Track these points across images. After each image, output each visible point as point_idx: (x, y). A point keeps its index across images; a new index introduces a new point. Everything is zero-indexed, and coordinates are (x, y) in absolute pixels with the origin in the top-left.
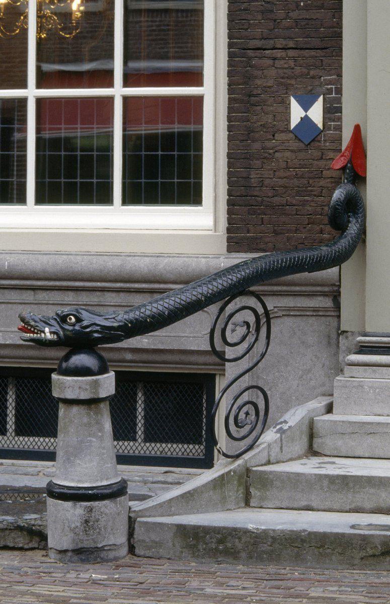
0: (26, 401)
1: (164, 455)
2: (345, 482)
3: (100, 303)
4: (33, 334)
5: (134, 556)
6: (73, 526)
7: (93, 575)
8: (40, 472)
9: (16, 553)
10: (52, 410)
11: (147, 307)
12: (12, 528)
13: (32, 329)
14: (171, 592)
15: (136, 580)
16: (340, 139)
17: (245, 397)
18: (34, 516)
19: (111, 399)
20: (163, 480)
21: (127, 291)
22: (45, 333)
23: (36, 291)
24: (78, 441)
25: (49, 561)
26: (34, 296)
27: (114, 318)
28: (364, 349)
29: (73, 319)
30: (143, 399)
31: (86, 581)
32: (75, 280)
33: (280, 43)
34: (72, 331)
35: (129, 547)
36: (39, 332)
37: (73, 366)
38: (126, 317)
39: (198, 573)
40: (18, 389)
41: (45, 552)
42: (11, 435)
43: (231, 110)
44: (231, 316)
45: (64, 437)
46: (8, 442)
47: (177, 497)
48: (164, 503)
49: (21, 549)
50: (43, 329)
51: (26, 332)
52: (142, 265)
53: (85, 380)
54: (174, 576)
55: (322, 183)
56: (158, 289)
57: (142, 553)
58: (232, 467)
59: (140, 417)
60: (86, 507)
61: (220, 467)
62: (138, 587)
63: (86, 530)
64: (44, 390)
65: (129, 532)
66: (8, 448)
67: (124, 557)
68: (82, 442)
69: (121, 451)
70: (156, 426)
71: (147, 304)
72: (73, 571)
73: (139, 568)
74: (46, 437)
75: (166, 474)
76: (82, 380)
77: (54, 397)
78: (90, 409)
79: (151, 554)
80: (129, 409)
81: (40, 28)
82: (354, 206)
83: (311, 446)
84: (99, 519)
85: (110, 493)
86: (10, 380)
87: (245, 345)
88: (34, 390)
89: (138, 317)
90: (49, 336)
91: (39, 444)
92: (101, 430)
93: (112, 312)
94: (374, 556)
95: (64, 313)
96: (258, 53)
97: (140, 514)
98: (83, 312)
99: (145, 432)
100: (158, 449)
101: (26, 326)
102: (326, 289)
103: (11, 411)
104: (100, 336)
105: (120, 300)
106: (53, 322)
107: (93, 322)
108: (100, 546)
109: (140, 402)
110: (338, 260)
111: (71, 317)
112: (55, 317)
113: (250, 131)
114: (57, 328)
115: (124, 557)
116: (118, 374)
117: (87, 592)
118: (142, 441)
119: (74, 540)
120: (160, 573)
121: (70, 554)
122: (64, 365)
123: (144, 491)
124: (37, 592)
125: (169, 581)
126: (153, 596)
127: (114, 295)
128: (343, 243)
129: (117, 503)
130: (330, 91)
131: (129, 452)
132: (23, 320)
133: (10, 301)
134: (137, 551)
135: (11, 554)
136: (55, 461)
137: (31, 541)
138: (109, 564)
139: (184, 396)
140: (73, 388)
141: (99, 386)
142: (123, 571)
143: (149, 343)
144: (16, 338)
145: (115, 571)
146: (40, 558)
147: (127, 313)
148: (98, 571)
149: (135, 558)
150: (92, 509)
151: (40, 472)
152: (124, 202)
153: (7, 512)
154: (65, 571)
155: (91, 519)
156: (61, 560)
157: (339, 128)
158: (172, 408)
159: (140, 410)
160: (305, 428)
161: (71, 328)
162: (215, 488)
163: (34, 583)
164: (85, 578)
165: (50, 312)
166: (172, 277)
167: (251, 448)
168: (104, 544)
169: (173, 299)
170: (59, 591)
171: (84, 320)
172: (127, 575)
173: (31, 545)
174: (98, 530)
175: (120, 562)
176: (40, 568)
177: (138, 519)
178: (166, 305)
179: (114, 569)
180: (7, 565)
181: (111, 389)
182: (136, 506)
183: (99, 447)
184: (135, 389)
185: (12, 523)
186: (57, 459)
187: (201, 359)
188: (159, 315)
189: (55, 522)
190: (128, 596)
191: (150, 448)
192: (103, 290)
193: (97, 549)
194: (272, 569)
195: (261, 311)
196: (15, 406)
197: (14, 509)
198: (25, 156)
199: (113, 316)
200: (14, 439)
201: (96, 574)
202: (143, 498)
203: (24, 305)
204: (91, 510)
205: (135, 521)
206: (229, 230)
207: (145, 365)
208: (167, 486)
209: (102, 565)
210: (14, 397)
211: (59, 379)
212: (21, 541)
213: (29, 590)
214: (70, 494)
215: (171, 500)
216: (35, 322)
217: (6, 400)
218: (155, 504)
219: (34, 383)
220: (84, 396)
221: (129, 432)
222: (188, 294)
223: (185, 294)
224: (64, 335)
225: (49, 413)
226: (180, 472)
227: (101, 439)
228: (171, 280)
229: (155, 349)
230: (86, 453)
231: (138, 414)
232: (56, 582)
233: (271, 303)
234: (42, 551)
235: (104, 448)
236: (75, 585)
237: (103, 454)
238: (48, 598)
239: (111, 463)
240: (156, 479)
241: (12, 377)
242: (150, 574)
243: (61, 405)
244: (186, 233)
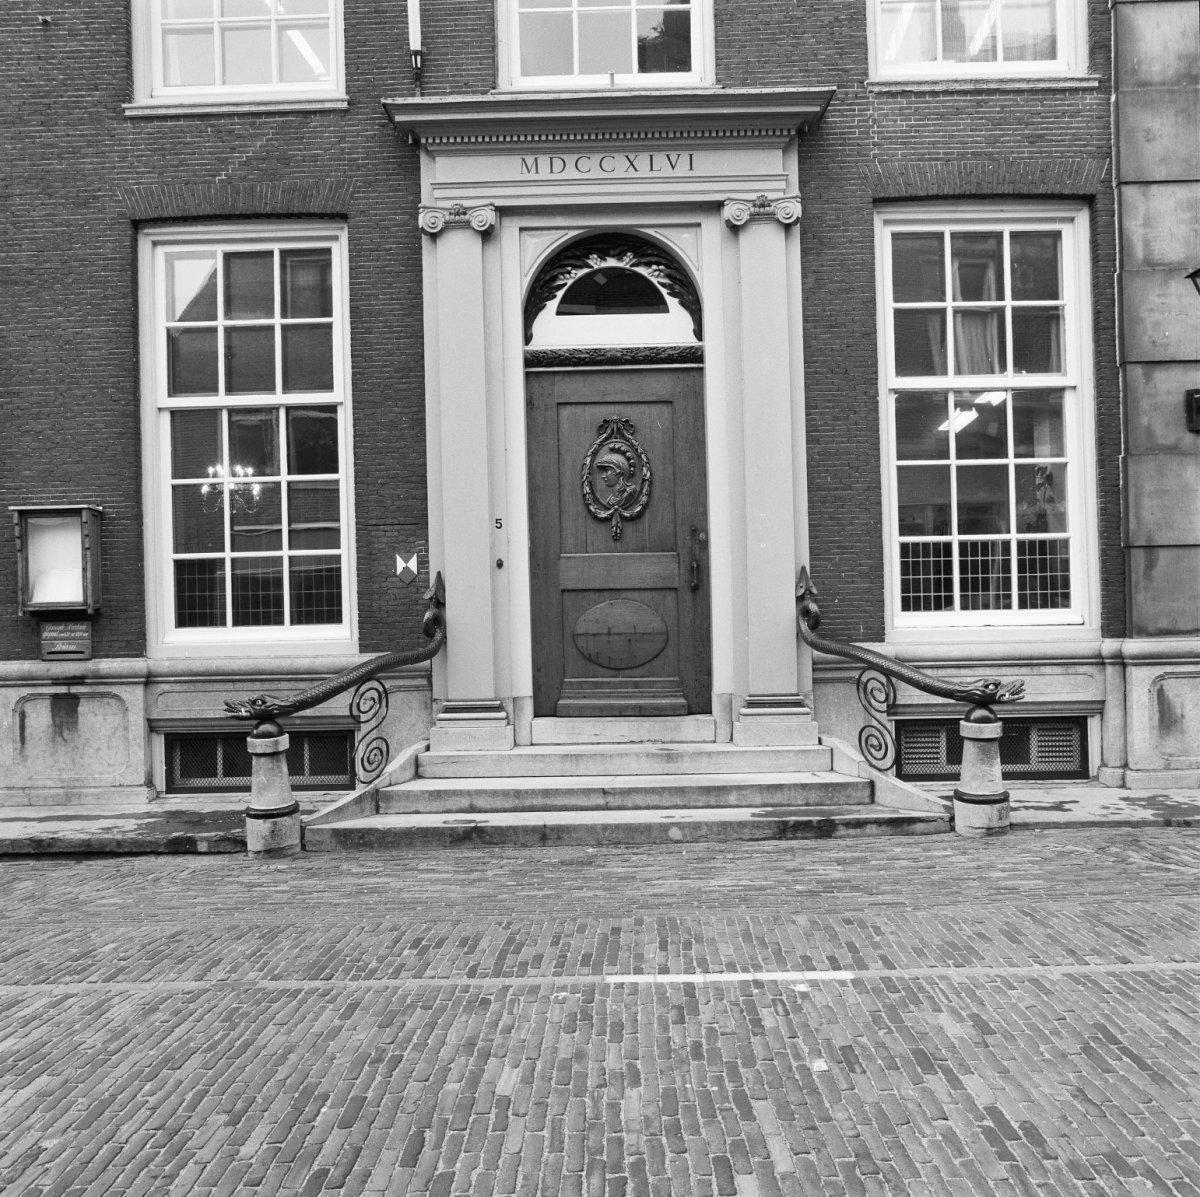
2: (438, 795)
16: (428, 580)
17: (374, 744)
19: (286, 752)
28: (448, 710)
33: (390, 521)
39: (347, 859)
43: (358, 563)
44: (363, 694)
49: (230, 853)
52: (304, 663)
61: (360, 789)
81: (232, 507)
82: (439, 621)
90: (244, 714)
92: (281, 772)
93: (286, 695)
110: (430, 655)
113: (371, 577)
114: (249, 708)
116: (167, 736)
123: (311, 807)
128: (432, 645)
130: (421, 551)
132: (227, 704)
152: (292, 623)
157: (428, 573)
158: (327, 752)
160: (413, 762)
165: (246, 697)
167: (378, 776)
182: (305, 818)
187: (345, 721)
194: (394, 853)
195: (381, 689)
198: (233, 591)
201: (281, 865)
202: (310, 812)
220: (269, 751)
230: (269, 787)
242: (317, 862)
244: (334, 643)
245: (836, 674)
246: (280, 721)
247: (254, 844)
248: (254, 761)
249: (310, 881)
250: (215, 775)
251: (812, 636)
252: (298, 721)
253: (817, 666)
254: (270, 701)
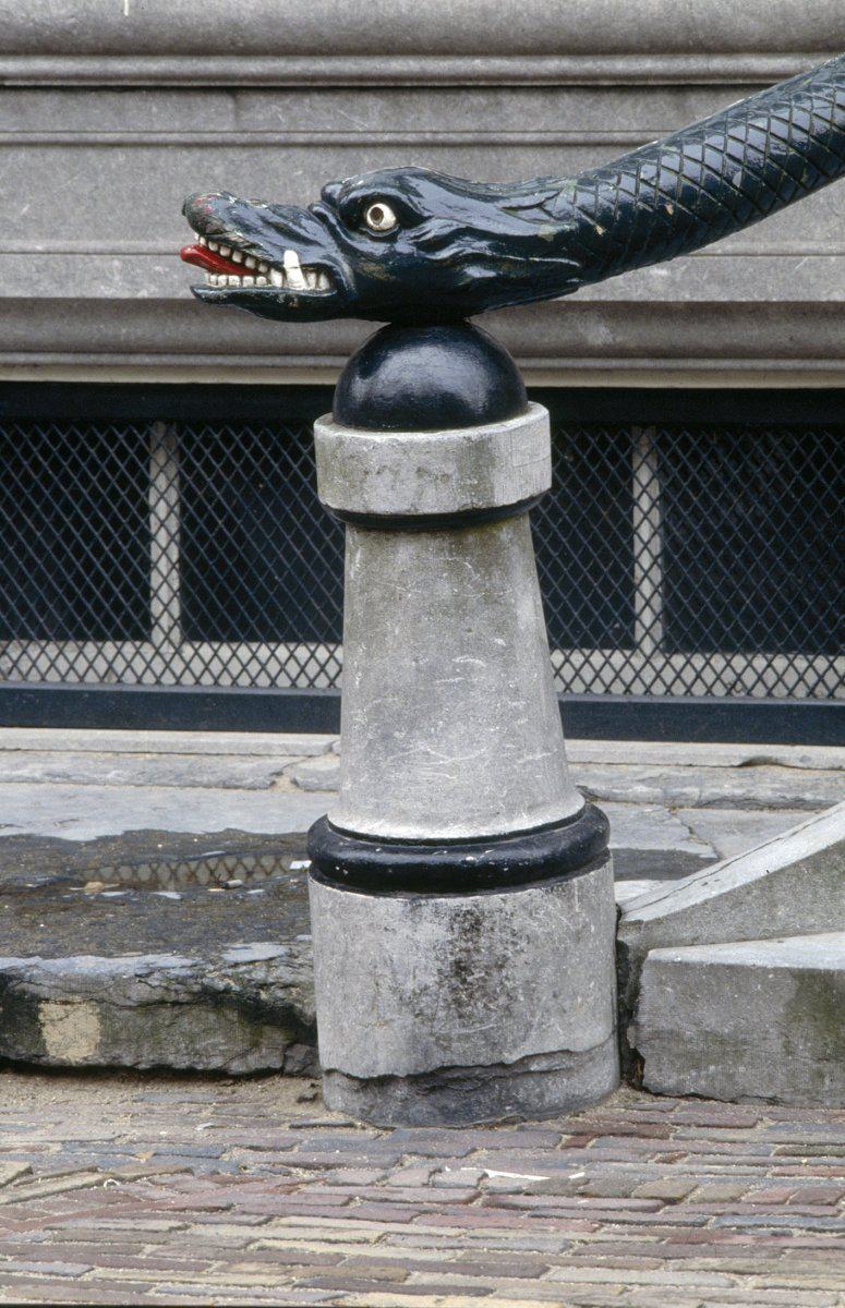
0: (220, 509)
1: (739, 697)
3: (484, 137)
4: (241, 276)
5: (639, 1094)
6: (410, 985)
7: (492, 1173)
8: (279, 774)
9: (201, 1091)
10: (318, 540)
11: (665, 160)
12: (183, 997)
13: (236, 258)
14: (784, 1235)
15: (651, 1188)
19: (537, 510)
20: (738, 792)
21: (586, 88)
22: (283, 272)
23: (246, 99)
24: (418, 670)
25: (325, 1119)
26: (237, 115)
27: (540, 206)
29: (389, 217)
30: (655, 491)
31: (463, 1195)
32: (390, 49)
34: (384, 259)
35: (622, 1058)
36: (262, 269)
37: (391, 392)
38: (586, 199)
40: (189, 467)
41: (308, 1083)
42: (167, 637)
45: (368, 655)
46: (158, 666)
47: (795, 865)
48: (747, 888)
49: (218, 1076)
50: (276, 257)
51: (212, 270)
53: (441, 443)
54: (793, 1169)
56: (704, 77)
57: (670, 1082)
59: (646, 560)
60: (456, 914)
62: (659, 1216)
63: (458, 1003)
64: (286, 467)
65: (620, 1002)
66: (157, 689)
67: (606, 1097)
68: (432, 672)
69: (578, 687)
70: (707, 588)
71: (663, 147)
72: (414, 1158)
73: (662, 1138)
74: (299, 642)
75: (750, 769)
76: (429, 443)
77: (319, 509)
78: (462, 549)
79: (702, 1085)
80: (605, 528)
84: (506, 959)
85: (544, 858)
86: (158, 432)
88: (247, 467)
89: (630, 199)
91: (273, 668)
93: (527, 177)
95: (353, 195)
97: (658, 932)
98: (424, 187)
99: (666, 616)
100: (718, 678)
101: (213, 247)
103: (164, 551)
104: (491, 274)
105: (561, 124)
106: (312, 229)
107: (464, 226)
108: (511, 1057)
109: (645, 503)
111: (380, 206)
112: (322, 210)
114: (327, 249)
115: (606, 1097)
117: (473, 1243)
118: (657, 647)
119: (414, 1039)
120: (739, 1159)
121: (401, 1091)
122: (360, 387)
123: (668, 839)
124: (283, 1245)
125: (777, 1192)
126: (716, 1255)
127: (535, 102)
129: (570, 897)
131: (607, 691)
132: (199, 223)
133: (146, 138)
134: (651, 1074)
135: (179, 1098)
136: (339, 733)
137: (255, 1045)
138: (549, 1124)
139: (808, 474)
140: (396, 473)
141: (494, 466)
142: (603, 1153)
143: (673, 283)
144: (182, 281)
145: (570, 1154)
146: (290, 1110)
147: (591, 184)
148: (510, 1154)
149: (647, 1101)
150: (478, 922)
151: (279, 774)
153: (160, 938)
154: (387, 1158)
155: (476, 957)
156: (368, 1118)
159: (645, 531)
161: (379, 249)
163: (270, 1209)
164: (459, 1187)
165: (303, 183)
166: (755, 29)
168: (526, 1049)
169: (762, 123)
170: (366, 1241)
171: (430, 217)
172: (616, 1170)
173: (254, 1062)
174: (502, 1000)
175: (585, 1119)
176: (290, 1148)
177: (652, 954)
178: (736, 149)
179: (566, 1147)
180: (170, 1141)
181: (536, 472)
182: (640, 897)
183: (499, 692)
184: (623, 456)
185: (181, 981)
186: (354, 609)
188: (712, 187)
189: (342, 973)
190: (623, 1253)
191: (689, 675)
192: (494, 86)
196: (181, 530)
197: (189, 925)
199: (538, 198)
200: (178, 651)
202: (673, 867)
203: (197, 153)
204: (476, 926)
205: (640, 960)
207: (662, 363)
208: (755, 815)
209: (522, 1129)
210: (173, 496)
211: (341, 442)
212: (218, 1044)
213: (252, 1241)
214: (397, 867)
215: (772, 878)
216: (247, 229)
217: (146, 510)
218: (715, 893)
219: (247, 440)
220: (436, 501)
221: (607, 616)
222: (817, 103)
223: (807, 104)
224: (357, 276)
225: (309, 554)
226: (802, 760)
227: (506, 658)
228: (753, 40)
229: (697, 303)
230: (446, 707)
231: (638, 546)
232: (352, 1205)
234: (294, 1081)
235: (516, 693)
236: (426, 1212)
237: (516, 715)
238: (323, 1270)
239: (546, 749)
240: (710, 791)
241: (168, 422)
242: (710, 1164)
243: (351, 537)
246: (497, 327)
247: (354, 1036)
248: (357, 557)
249: (667, 1276)
250: (137, 627)
252: (599, 334)
254: (441, 213)
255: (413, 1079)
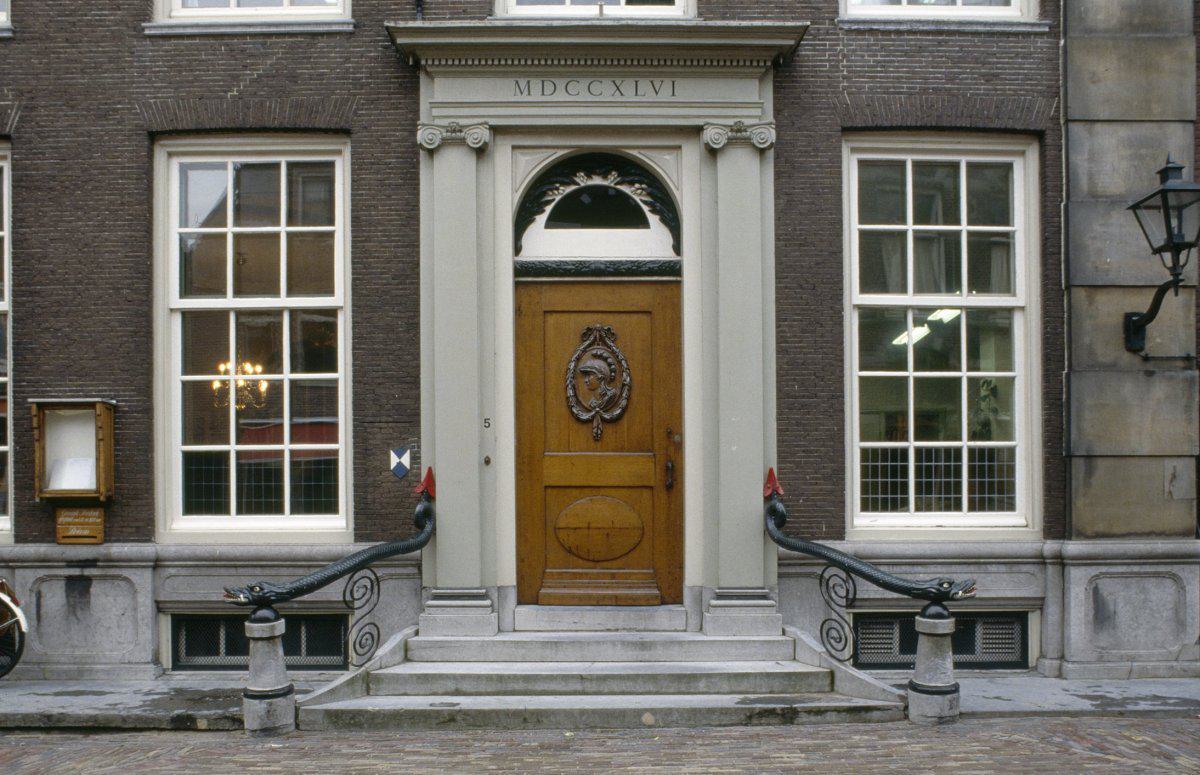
17: (367, 629)
18: (236, 709)
19: (283, 637)
29: (258, 589)
32: (261, 560)
33: (384, 419)
39: (338, 739)
43: (355, 458)
49: (228, 730)
52: (303, 551)
55: (410, 500)
58: (359, 671)
82: (429, 514)
83: (406, 656)
87: (366, 597)
93: (284, 582)
94: (444, 722)
96: (371, 425)
102: (413, 563)
110: (420, 546)
113: (367, 470)
128: (423, 536)
132: (227, 590)
144: (221, 598)
157: (419, 469)
158: (321, 634)
160: (402, 646)
162: (348, 685)
165: (246, 582)
166: (321, 558)
167: (369, 660)
182: (299, 698)
186: (251, 652)
193: (276, 728)
194: (383, 733)
195: (373, 577)
202: (306, 692)
206: (355, 529)
212: (228, 725)
233: (380, 573)
242: (309, 742)
244: (328, 530)
245: (798, 570)
250: (217, 653)
251: (778, 534)
252: (296, 606)
253: (782, 562)
255: (261, 730)
